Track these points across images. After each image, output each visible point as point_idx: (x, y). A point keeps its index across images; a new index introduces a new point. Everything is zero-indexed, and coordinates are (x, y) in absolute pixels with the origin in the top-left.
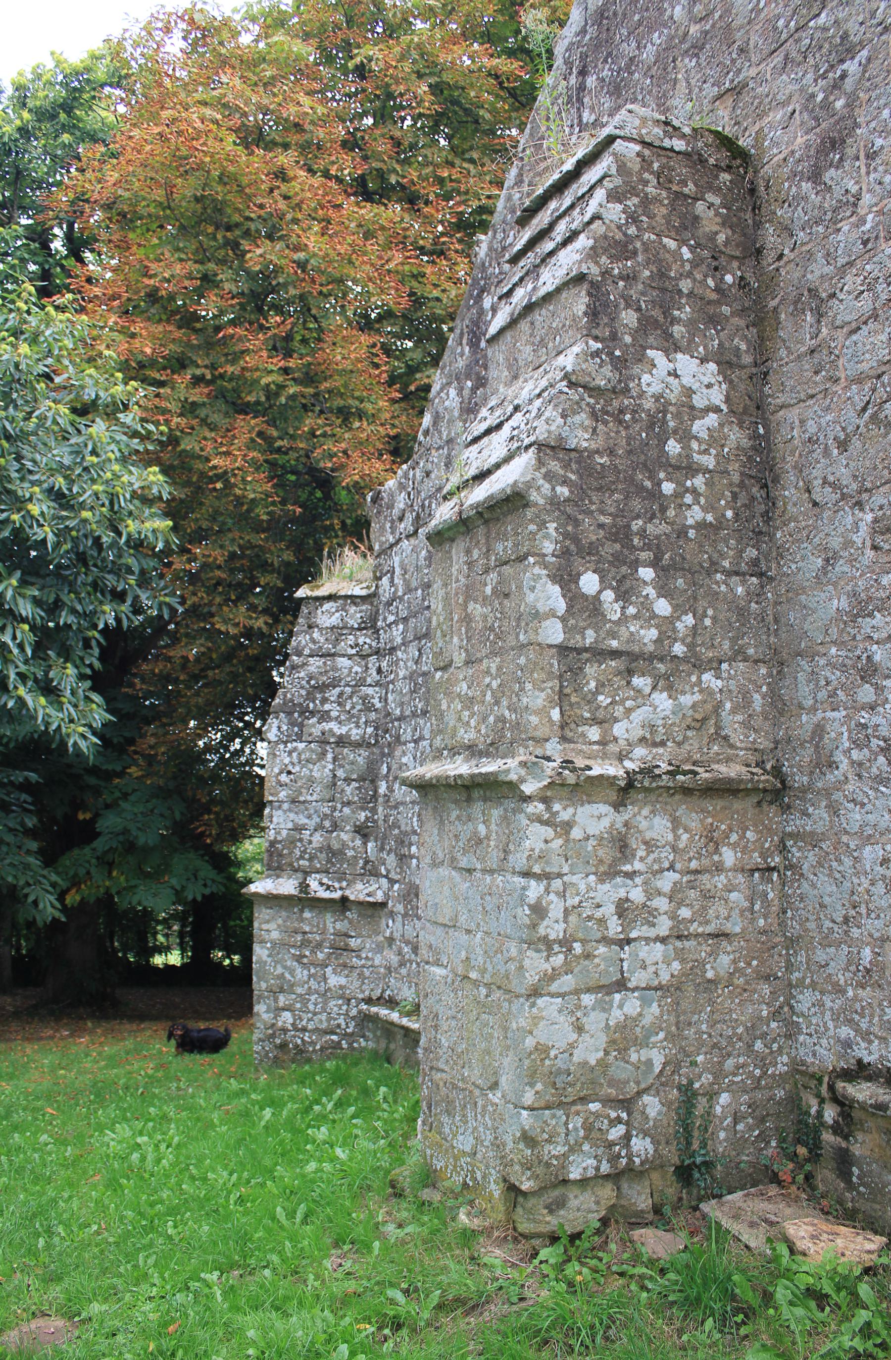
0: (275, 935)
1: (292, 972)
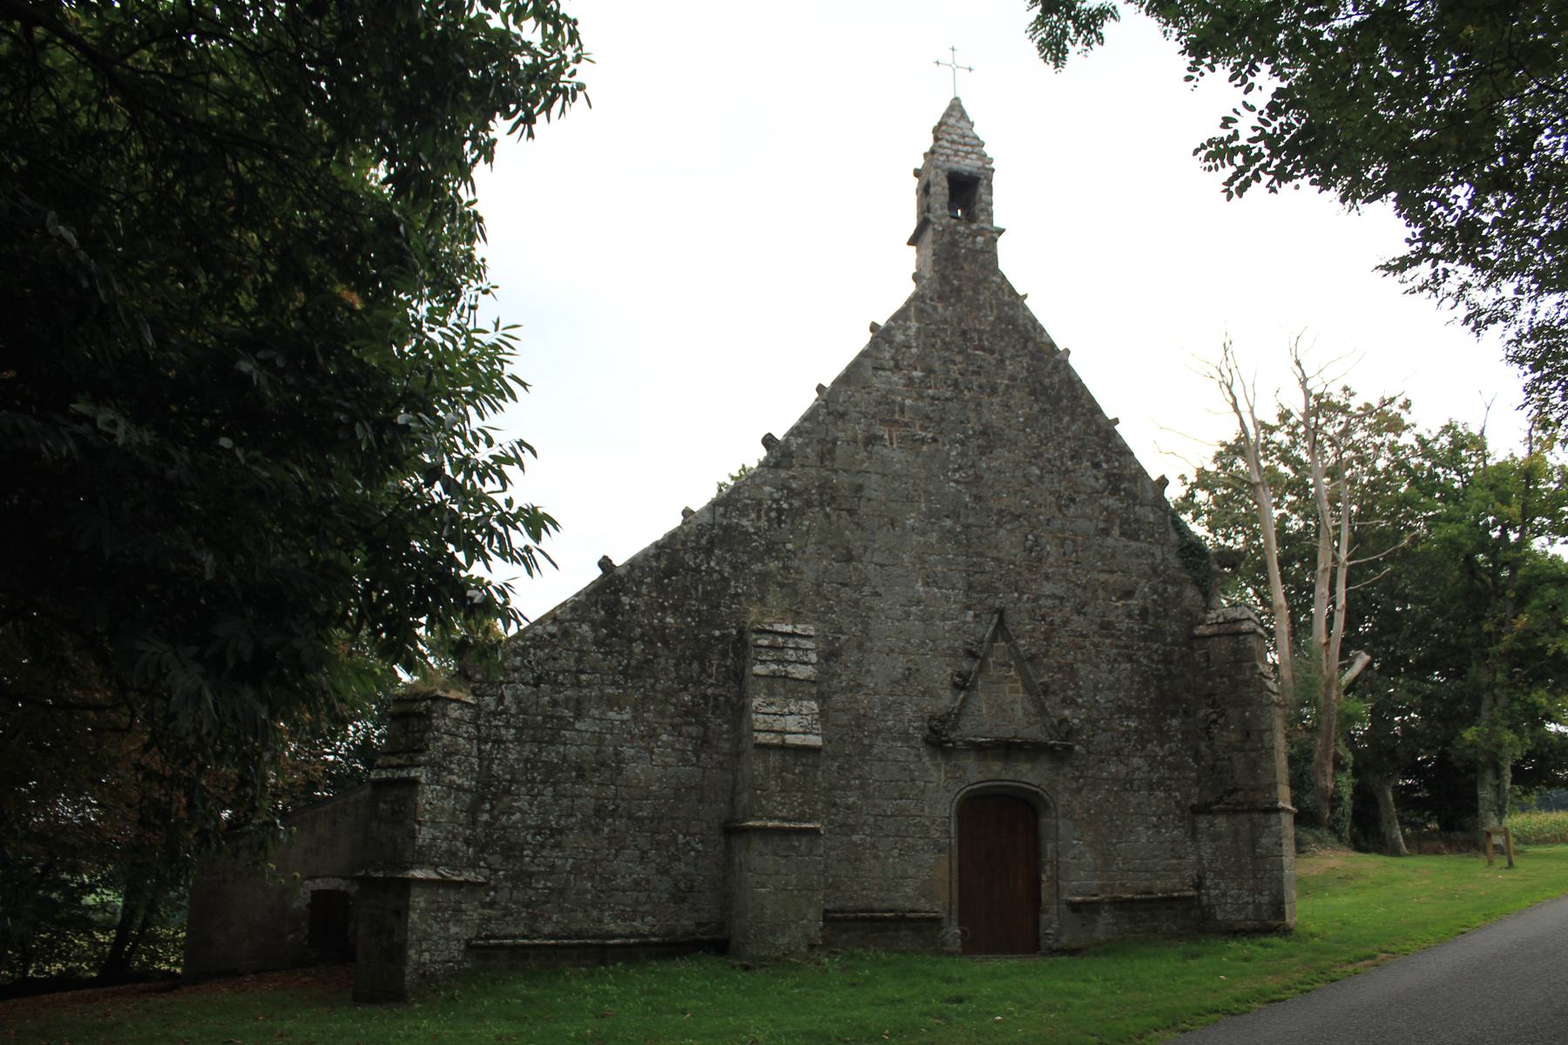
0: (422, 905)
1: (431, 927)
